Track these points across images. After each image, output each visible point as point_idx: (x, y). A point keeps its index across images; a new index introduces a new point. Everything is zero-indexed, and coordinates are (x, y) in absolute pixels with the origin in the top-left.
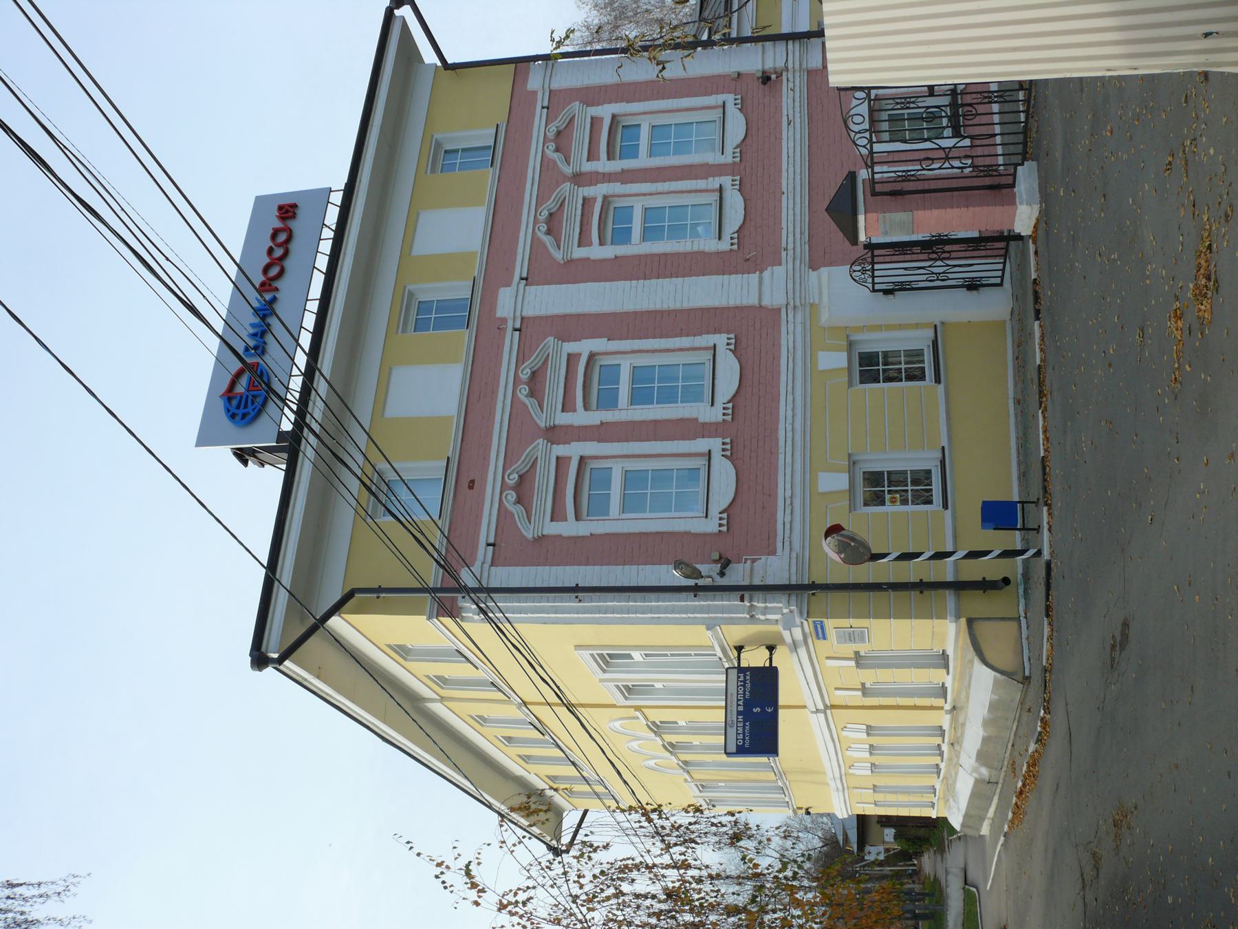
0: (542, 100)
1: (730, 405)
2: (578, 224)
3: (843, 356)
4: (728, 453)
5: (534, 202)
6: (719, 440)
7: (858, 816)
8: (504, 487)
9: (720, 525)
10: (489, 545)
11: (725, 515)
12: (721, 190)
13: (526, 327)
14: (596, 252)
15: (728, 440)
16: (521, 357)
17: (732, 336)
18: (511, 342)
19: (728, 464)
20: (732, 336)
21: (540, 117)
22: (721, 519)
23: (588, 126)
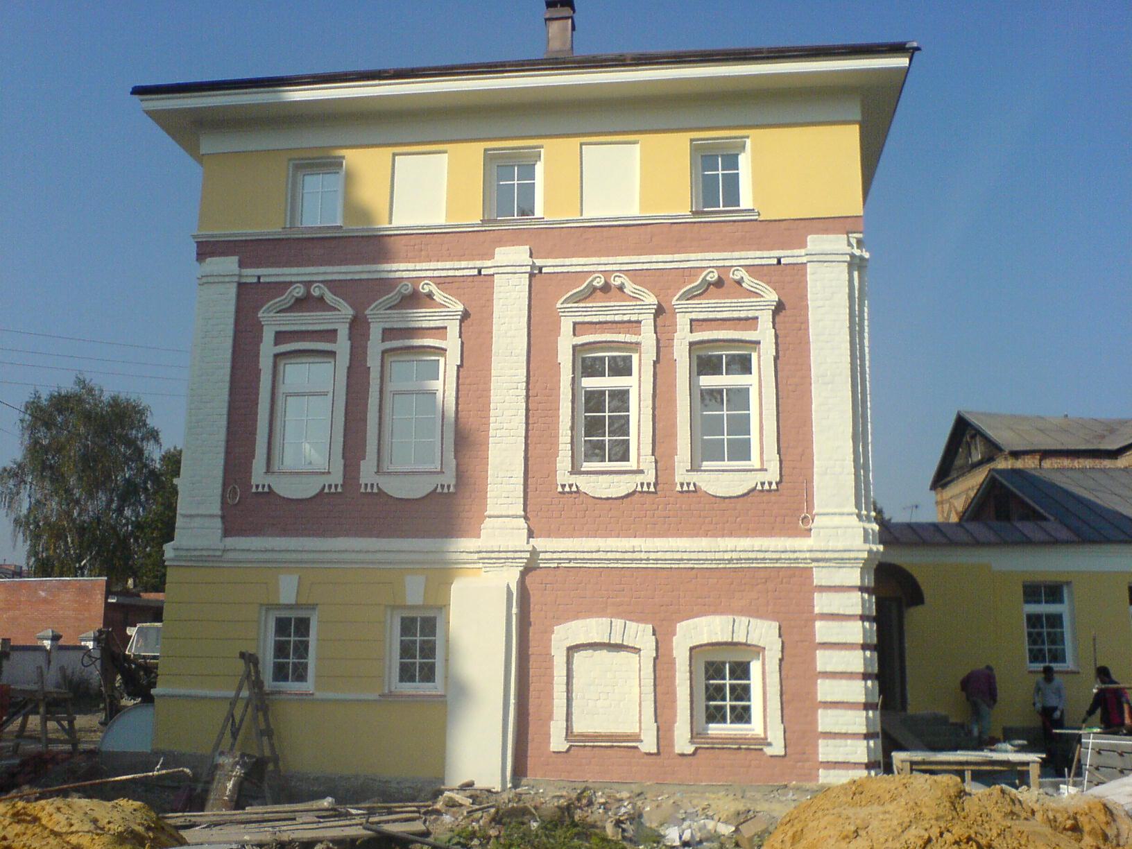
0: (790, 256)
1: (375, 490)
2: (602, 319)
3: (419, 601)
4: (326, 490)
5: (436, 274)
6: (340, 482)
7: (162, 608)
8: (308, 284)
9: (563, 486)
10: (259, 277)
11: (692, 488)
12: (642, 472)
13: (483, 281)
14: (566, 343)
15: (339, 490)
16: (442, 280)
17: (452, 489)
18: (466, 267)
19: (430, 489)
20: (339, 490)
21: (767, 257)
22: (688, 484)
23: (743, 315)
